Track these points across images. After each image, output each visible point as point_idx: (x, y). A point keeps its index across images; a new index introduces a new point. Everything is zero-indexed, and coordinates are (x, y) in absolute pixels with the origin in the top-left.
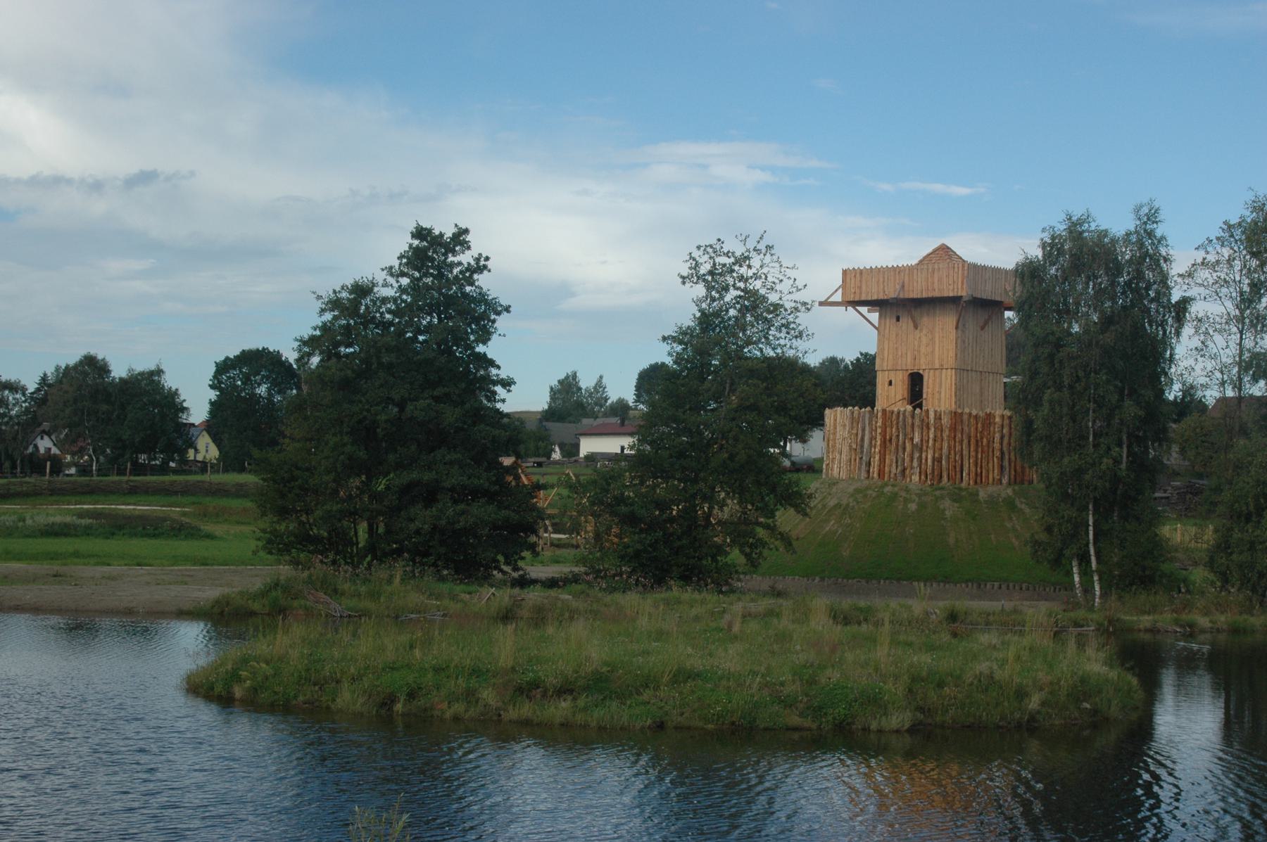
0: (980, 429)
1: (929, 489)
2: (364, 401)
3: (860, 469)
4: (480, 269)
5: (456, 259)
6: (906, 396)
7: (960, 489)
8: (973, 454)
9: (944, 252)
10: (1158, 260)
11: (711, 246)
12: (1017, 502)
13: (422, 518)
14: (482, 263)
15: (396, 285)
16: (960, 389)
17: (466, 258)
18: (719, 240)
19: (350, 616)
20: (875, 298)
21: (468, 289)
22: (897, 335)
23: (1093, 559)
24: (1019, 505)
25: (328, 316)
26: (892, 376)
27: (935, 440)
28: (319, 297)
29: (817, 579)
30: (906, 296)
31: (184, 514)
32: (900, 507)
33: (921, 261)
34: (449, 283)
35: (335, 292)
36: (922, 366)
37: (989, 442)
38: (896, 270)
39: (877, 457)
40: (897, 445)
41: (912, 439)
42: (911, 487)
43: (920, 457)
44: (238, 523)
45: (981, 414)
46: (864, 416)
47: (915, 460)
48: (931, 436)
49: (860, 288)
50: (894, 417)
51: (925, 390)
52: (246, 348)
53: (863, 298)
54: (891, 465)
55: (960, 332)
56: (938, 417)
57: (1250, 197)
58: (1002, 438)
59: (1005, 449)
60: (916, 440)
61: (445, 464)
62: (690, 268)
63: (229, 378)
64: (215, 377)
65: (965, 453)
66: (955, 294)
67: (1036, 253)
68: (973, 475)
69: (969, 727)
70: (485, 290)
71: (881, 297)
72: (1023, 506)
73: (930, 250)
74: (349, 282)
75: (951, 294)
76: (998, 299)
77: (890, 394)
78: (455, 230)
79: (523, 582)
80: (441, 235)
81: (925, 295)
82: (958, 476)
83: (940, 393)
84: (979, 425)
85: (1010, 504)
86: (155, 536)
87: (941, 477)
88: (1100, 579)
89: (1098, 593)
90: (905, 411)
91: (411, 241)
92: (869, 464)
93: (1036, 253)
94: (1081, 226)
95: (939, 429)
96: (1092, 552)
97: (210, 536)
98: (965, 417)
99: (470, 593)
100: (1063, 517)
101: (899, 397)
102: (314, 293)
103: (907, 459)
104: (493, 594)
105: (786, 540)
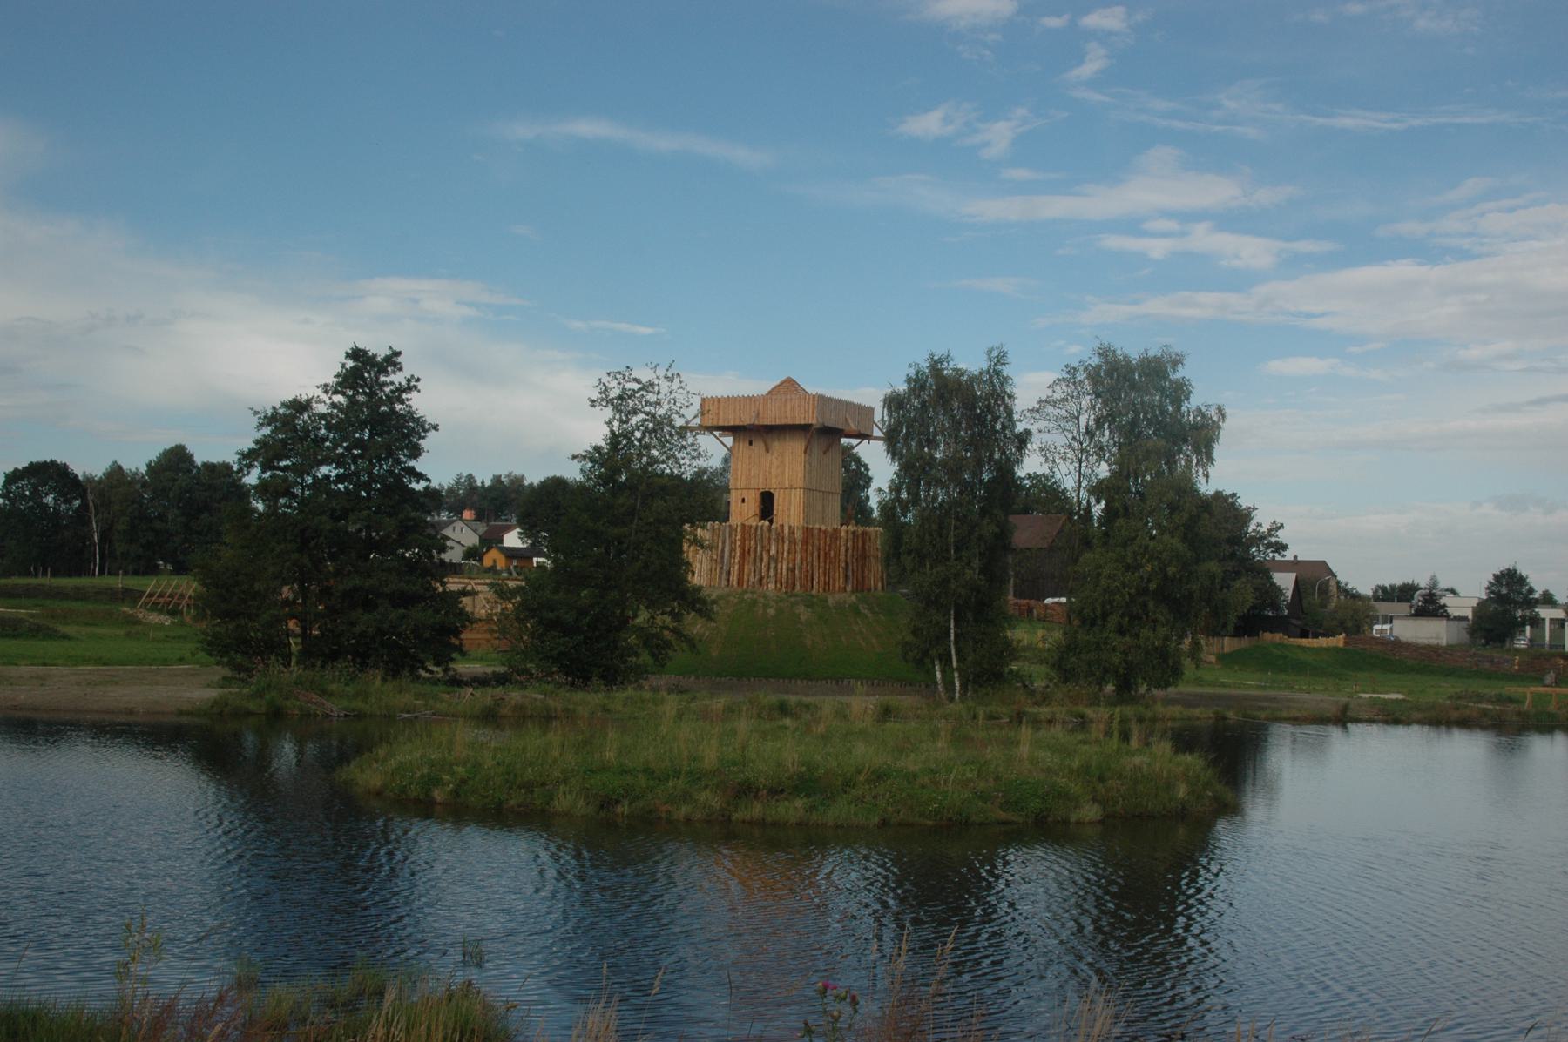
0: (828, 542)
1: (784, 596)
2: (307, 510)
3: (720, 577)
4: (409, 389)
5: (388, 379)
6: (758, 512)
7: (812, 596)
8: (822, 564)
9: (789, 385)
10: (1003, 397)
11: (620, 373)
12: (861, 608)
13: (365, 622)
14: (413, 383)
15: (328, 402)
16: (808, 507)
17: (398, 378)
18: (628, 367)
19: (346, 715)
20: (732, 423)
21: (398, 407)
22: (750, 457)
23: (954, 659)
24: (862, 611)
25: (267, 431)
26: (745, 494)
27: (789, 552)
28: (256, 413)
29: (693, 678)
30: (761, 423)
31: (32, 616)
32: (761, 612)
33: (770, 392)
34: (381, 402)
35: (274, 408)
36: (772, 486)
37: (835, 554)
38: (752, 399)
39: (736, 567)
40: (755, 556)
41: (769, 551)
42: (768, 593)
43: (776, 568)
44: (87, 624)
45: (829, 529)
46: (724, 531)
47: (772, 570)
48: (786, 548)
49: (718, 414)
50: (753, 531)
51: (775, 507)
52: (35, 460)
53: (721, 423)
54: (749, 575)
55: (807, 457)
56: (792, 532)
57: (1097, 344)
58: (847, 551)
59: (849, 560)
60: (773, 552)
61: (383, 570)
62: (600, 393)
63: (17, 488)
64: (4, 486)
65: (815, 564)
66: (806, 422)
67: (902, 388)
68: (822, 584)
69: (1138, 816)
70: (414, 409)
71: (738, 423)
72: (866, 611)
73: (778, 382)
74: (290, 397)
75: (803, 422)
76: (840, 427)
77: (743, 511)
78: (388, 352)
79: (456, 682)
80: (374, 356)
81: (778, 422)
82: (810, 584)
83: (789, 510)
84: (828, 539)
85: (855, 609)
86: (15, 637)
87: (794, 584)
88: (960, 676)
89: (958, 688)
90: (762, 526)
91: (344, 361)
92: (729, 573)
93: (902, 388)
94: (942, 364)
95: (793, 542)
96: (953, 652)
97: (66, 637)
98: (816, 532)
99: (449, 693)
100: (931, 622)
101: (752, 513)
102: (252, 409)
103: (764, 569)
104: (472, 694)
105: (691, 643)
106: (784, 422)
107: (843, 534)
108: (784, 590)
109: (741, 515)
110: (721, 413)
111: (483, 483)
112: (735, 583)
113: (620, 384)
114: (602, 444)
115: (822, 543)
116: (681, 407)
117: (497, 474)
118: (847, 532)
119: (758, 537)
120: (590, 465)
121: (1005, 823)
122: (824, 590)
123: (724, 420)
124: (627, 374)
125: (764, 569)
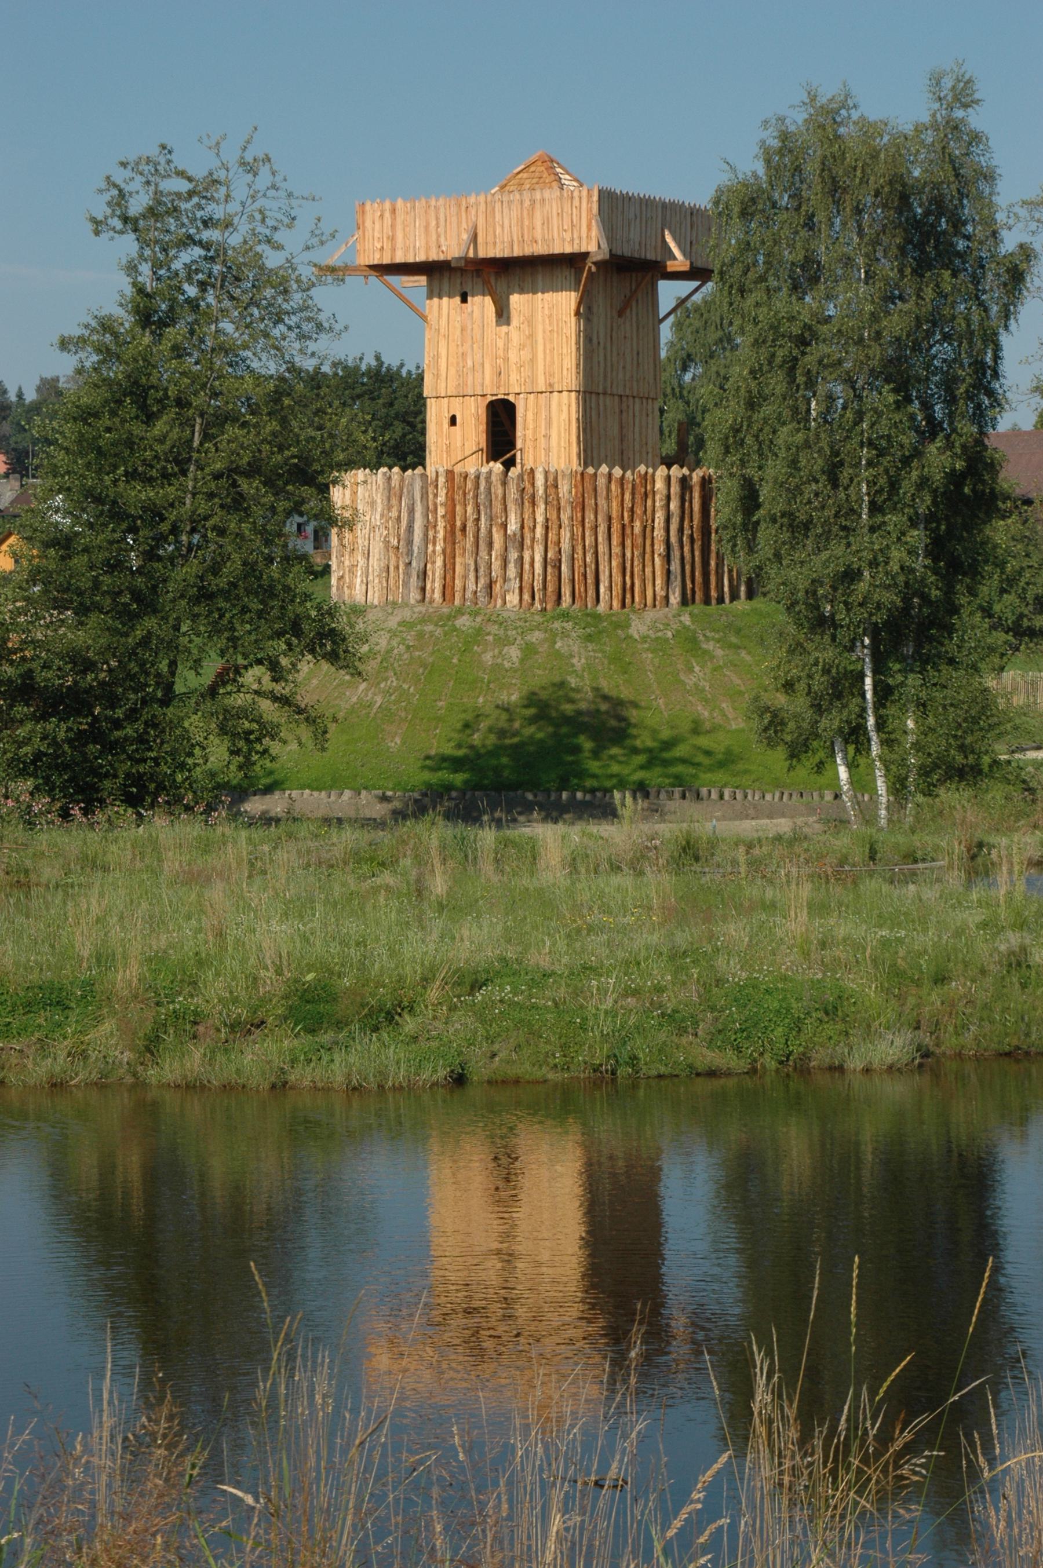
3: (406, 584)
6: (483, 445)
8: (616, 550)
11: (148, 161)
18: (164, 147)
20: (421, 258)
36: (512, 388)
39: (439, 562)
41: (504, 526)
49: (392, 239)
50: (470, 485)
53: (399, 258)
54: (465, 577)
56: (552, 484)
60: (513, 527)
65: (602, 548)
66: (576, 249)
68: (617, 590)
69: (1008, 1054)
71: (434, 256)
75: (568, 250)
81: (517, 252)
82: (591, 592)
83: (548, 437)
90: (490, 472)
95: (553, 501)
101: (471, 446)
103: (496, 565)
106: (528, 250)
107: (659, 485)
108: (538, 606)
109: (448, 452)
110: (400, 235)
111: (20, 396)
112: (437, 595)
113: (148, 183)
114: (120, 312)
115: (615, 505)
116: (275, 229)
117: (48, 375)
118: (668, 479)
119: (482, 498)
120: (95, 358)
121: (712, 1074)
122: (623, 606)
123: (406, 250)
124: (162, 160)
125: (496, 565)
